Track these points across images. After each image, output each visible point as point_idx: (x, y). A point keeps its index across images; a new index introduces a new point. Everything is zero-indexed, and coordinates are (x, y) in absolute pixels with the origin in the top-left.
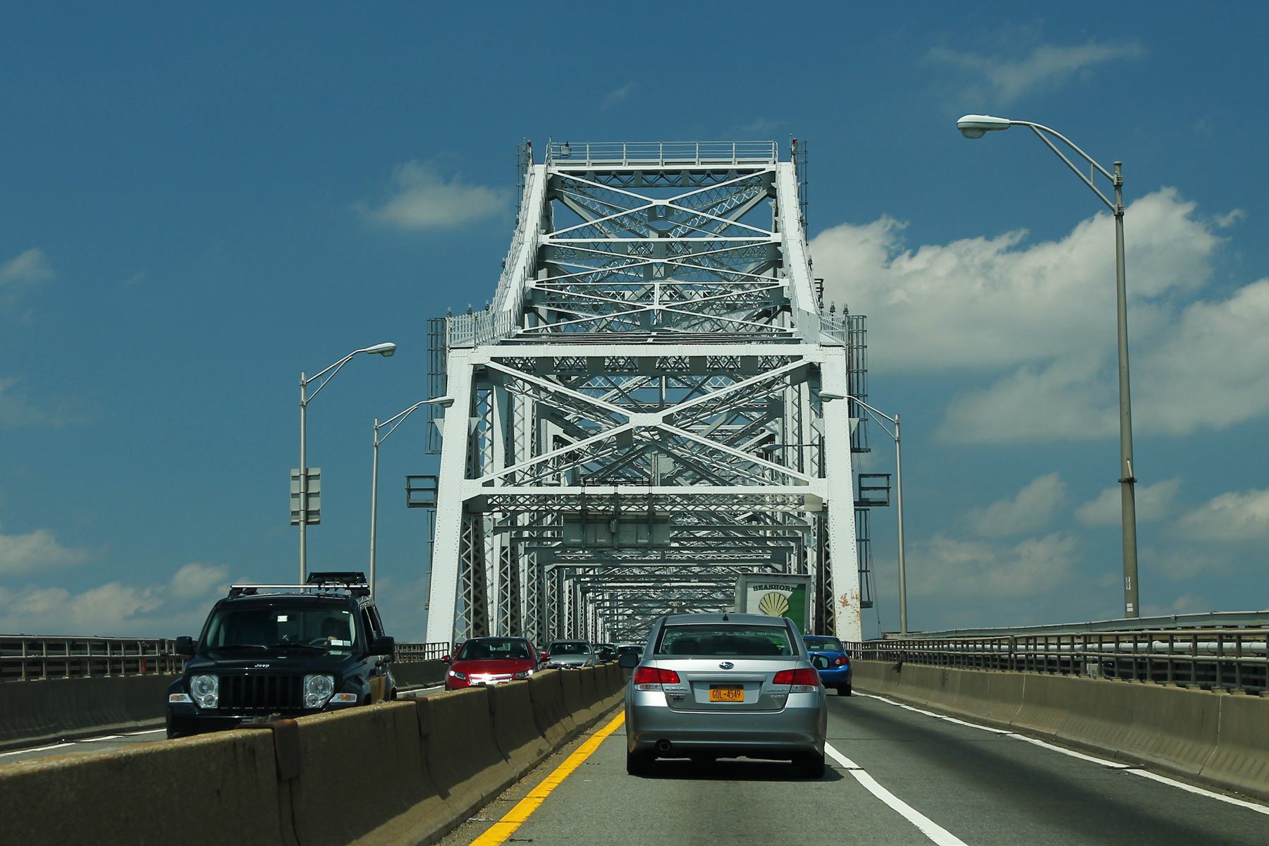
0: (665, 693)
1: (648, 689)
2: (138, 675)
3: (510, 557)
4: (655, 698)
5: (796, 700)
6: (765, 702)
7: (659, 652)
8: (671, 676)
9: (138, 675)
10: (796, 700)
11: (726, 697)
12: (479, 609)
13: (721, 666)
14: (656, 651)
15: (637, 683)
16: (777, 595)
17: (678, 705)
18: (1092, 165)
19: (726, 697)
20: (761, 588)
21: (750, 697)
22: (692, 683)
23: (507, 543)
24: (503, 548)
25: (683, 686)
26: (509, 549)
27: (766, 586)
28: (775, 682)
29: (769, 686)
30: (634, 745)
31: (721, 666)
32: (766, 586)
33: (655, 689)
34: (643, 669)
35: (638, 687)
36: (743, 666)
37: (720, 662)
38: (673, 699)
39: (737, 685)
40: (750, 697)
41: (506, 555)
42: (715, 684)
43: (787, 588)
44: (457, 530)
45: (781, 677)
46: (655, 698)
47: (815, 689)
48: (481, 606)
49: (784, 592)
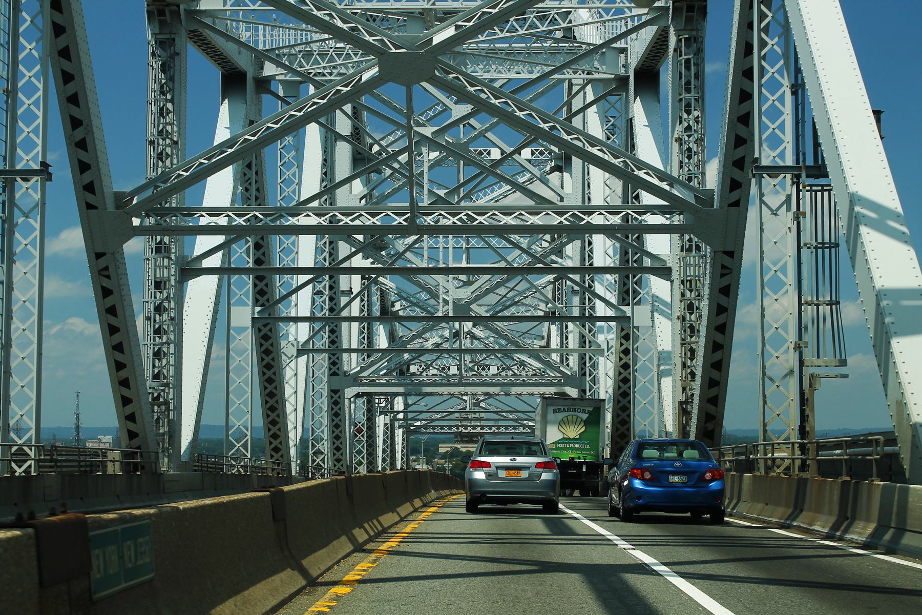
0: (485, 473)
1: (476, 470)
2: (98, 473)
3: (390, 429)
4: (479, 475)
5: (546, 476)
6: (531, 477)
7: (480, 454)
8: (488, 465)
9: (98, 473)
10: (546, 476)
11: (513, 474)
12: (333, 285)
13: (511, 460)
14: (480, 453)
15: (471, 468)
16: (575, 418)
17: (490, 478)
18: (763, 81)
19: (513, 474)
20: (559, 411)
21: (524, 474)
22: (497, 468)
23: (388, 421)
24: (385, 425)
25: (493, 469)
26: (389, 425)
27: (564, 409)
28: (536, 468)
29: (533, 469)
30: (469, 497)
31: (511, 460)
32: (564, 409)
33: (479, 471)
34: (474, 461)
35: (472, 470)
36: (521, 460)
37: (510, 458)
38: (489, 475)
39: (519, 468)
40: (524, 474)
41: (387, 428)
42: (507, 468)
43: (584, 411)
44: (223, 115)
45: (538, 465)
46: (479, 475)
47: (554, 471)
48: (393, 461)
49: (580, 415)
